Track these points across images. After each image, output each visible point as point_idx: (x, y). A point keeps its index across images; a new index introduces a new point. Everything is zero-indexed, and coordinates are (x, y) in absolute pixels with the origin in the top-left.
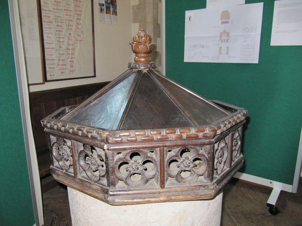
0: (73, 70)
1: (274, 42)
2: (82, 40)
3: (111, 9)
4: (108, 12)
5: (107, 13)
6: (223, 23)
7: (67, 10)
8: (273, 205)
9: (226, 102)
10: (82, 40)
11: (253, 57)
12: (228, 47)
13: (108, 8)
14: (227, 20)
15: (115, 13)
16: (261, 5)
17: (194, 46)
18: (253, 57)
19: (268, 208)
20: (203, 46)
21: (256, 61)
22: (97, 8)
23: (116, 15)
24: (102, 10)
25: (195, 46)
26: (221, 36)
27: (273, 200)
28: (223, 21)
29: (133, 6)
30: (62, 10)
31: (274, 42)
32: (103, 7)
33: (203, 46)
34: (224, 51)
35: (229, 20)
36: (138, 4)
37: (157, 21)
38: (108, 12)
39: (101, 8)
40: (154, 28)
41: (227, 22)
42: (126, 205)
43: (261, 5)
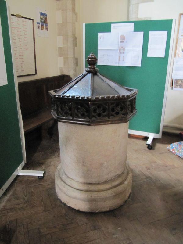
0: (23, 69)
1: (166, 33)
2: (27, 49)
3: (44, 26)
4: (42, 28)
5: (42, 29)
6: (121, 42)
7: (18, 28)
8: (149, 145)
9: (128, 87)
10: (27, 49)
11: (138, 64)
12: (124, 57)
13: (42, 26)
14: (123, 41)
15: (47, 29)
16: (142, 33)
17: (104, 55)
18: (138, 64)
19: (147, 146)
20: (109, 56)
21: (140, 66)
22: (36, 25)
23: (47, 30)
24: (39, 27)
25: (104, 55)
26: (120, 50)
27: (149, 142)
28: (121, 41)
29: (58, 24)
30: (15, 28)
31: (166, 33)
32: (39, 25)
33: (109, 55)
34: (122, 58)
35: (125, 41)
36: (61, 22)
37: (75, 35)
38: (42, 28)
39: (38, 26)
40: (73, 40)
41: (123, 42)
42: (175, 31)
43: (142, 33)
